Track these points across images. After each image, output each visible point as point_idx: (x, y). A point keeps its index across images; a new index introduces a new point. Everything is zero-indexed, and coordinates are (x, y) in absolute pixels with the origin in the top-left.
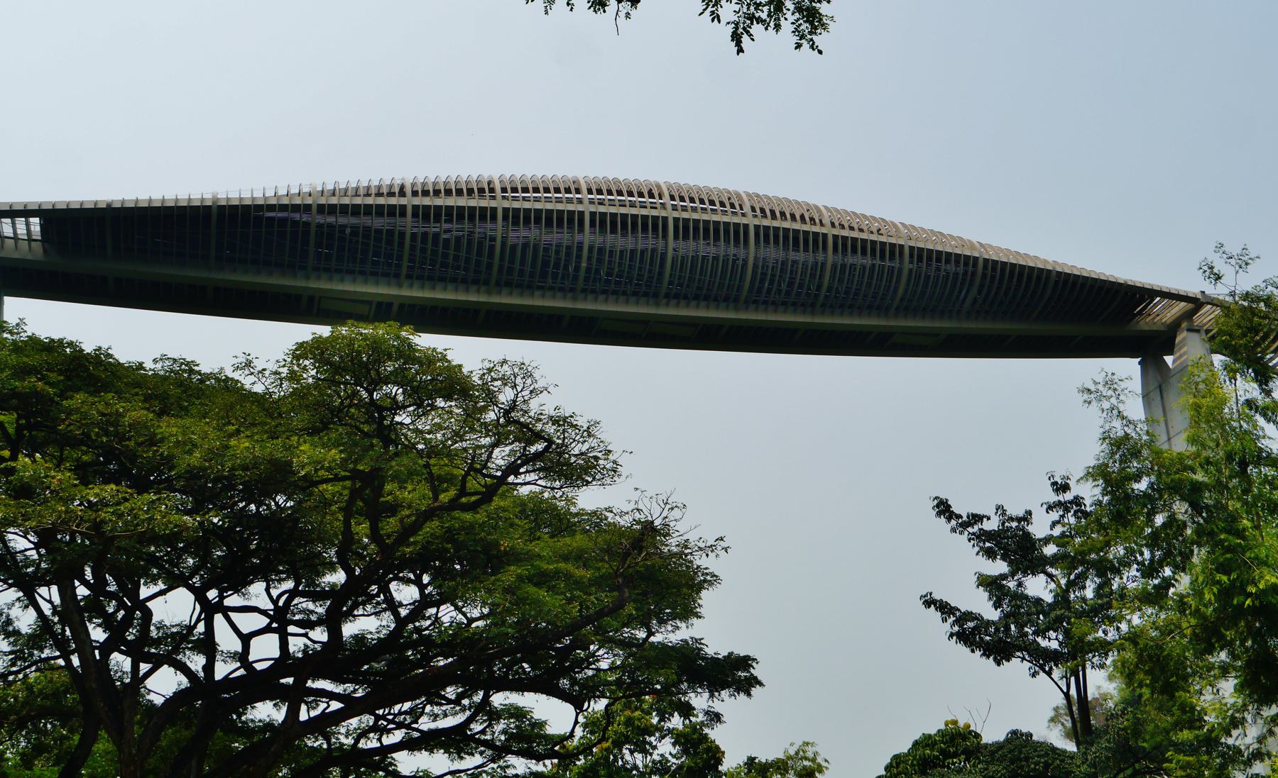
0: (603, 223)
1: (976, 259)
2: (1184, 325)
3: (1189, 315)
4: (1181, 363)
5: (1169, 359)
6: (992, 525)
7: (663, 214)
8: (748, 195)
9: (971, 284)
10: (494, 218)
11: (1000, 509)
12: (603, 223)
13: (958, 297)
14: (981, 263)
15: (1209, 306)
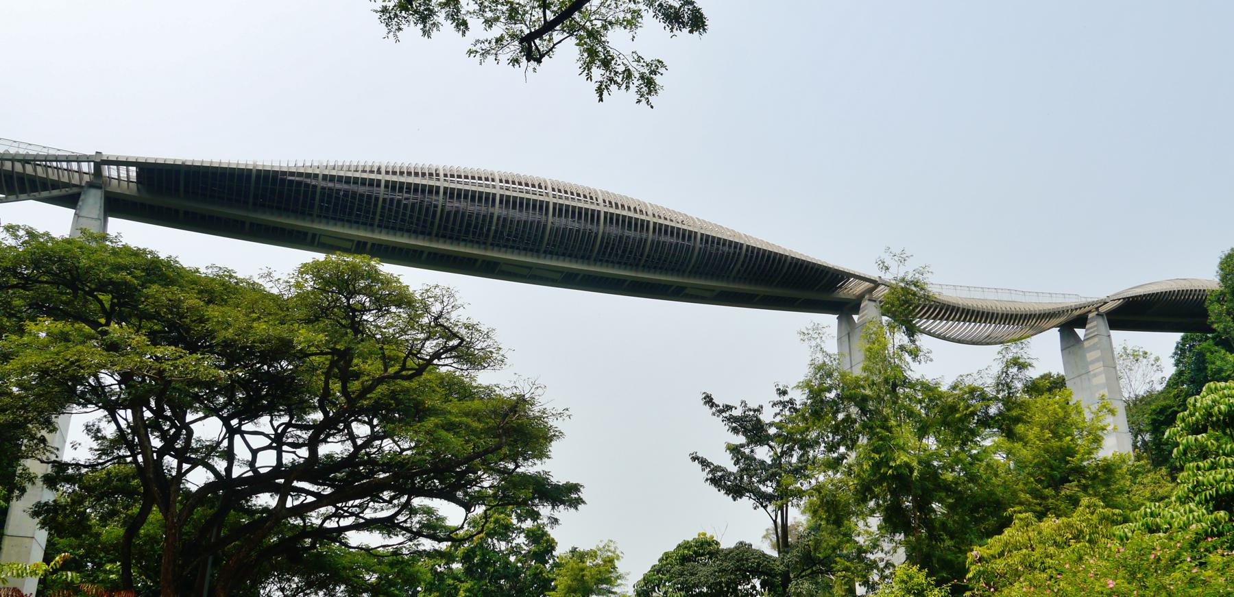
1: (742, 245)
2: (867, 297)
3: (870, 291)
5: (855, 317)
6: (737, 413)
8: (602, 192)
11: (744, 403)
13: (729, 267)
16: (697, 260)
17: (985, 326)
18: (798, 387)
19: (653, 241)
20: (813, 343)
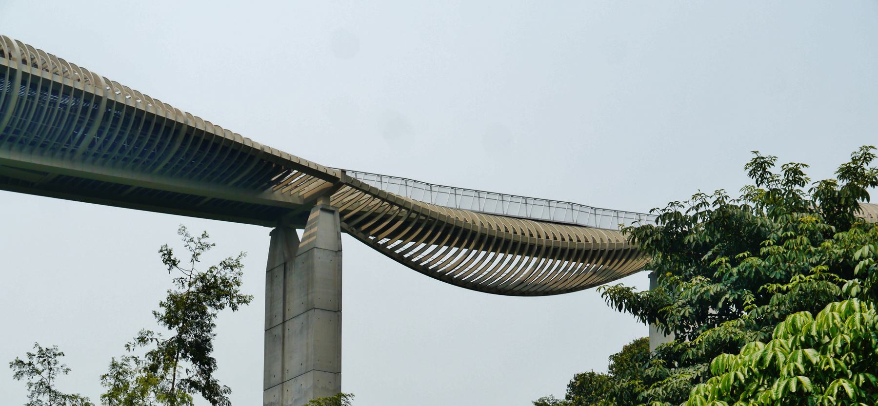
1: (99, 99)
2: (320, 203)
3: (326, 194)
4: (309, 243)
5: (300, 233)
9: (90, 124)
13: (74, 135)
14: (184, 131)
15: (348, 188)
16: (13, 120)
17: (468, 254)
18: (244, 300)
20: (36, 379)
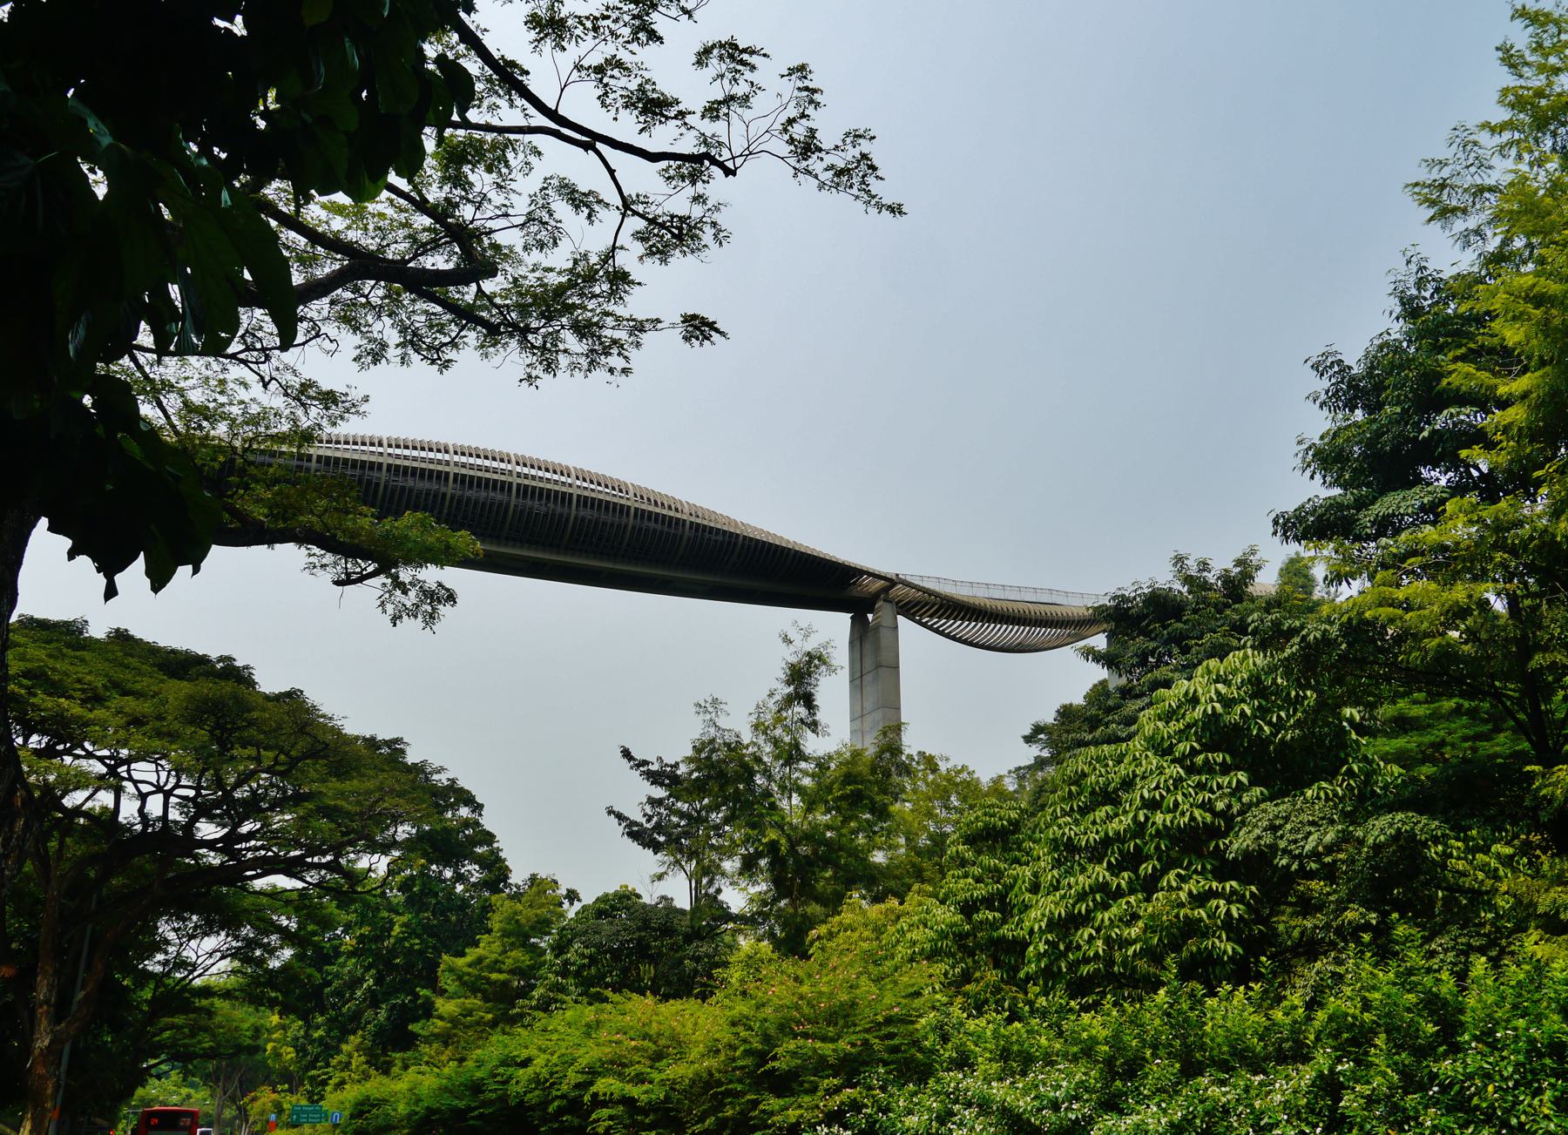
0: (463, 481)
1: (738, 535)
3: (886, 590)
6: (655, 767)
7: (510, 479)
8: (575, 469)
10: (447, 478)
11: (660, 759)
12: (463, 481)
19: (634, 527)
20: (708, 717)
